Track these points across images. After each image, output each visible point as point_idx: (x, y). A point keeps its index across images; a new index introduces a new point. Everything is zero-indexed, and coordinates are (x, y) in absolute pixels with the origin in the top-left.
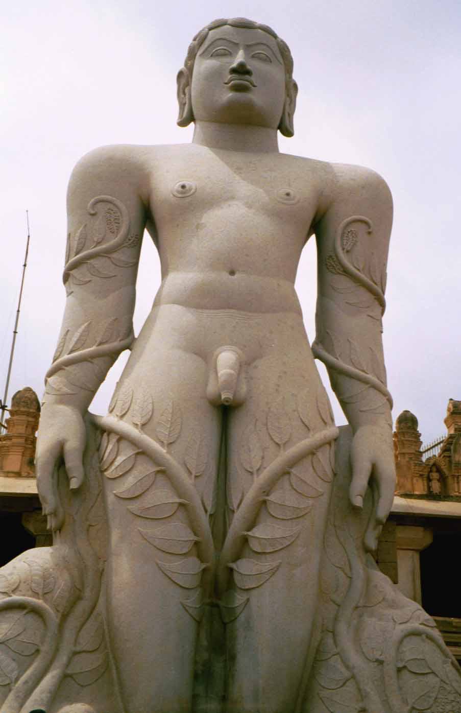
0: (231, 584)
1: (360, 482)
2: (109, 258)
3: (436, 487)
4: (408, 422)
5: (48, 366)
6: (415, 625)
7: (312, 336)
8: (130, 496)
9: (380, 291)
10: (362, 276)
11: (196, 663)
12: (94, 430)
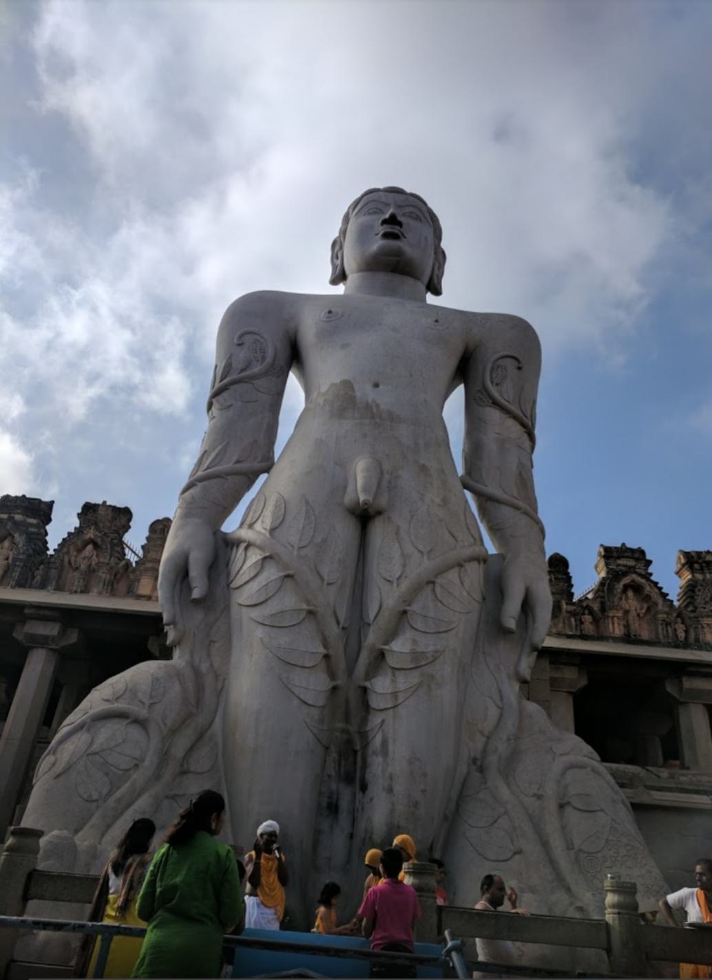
0: (366, 707)
1: (512, 608)
2: (253, 384)
3: (589, 627)
4: (559, 565)
5: (184, 482)
6: (580, 759)
7: (460, 471)
8: (253, 603)
9: (530, 424)
10: (513, 408)
11: (320, 794)
12: (224, 547)
